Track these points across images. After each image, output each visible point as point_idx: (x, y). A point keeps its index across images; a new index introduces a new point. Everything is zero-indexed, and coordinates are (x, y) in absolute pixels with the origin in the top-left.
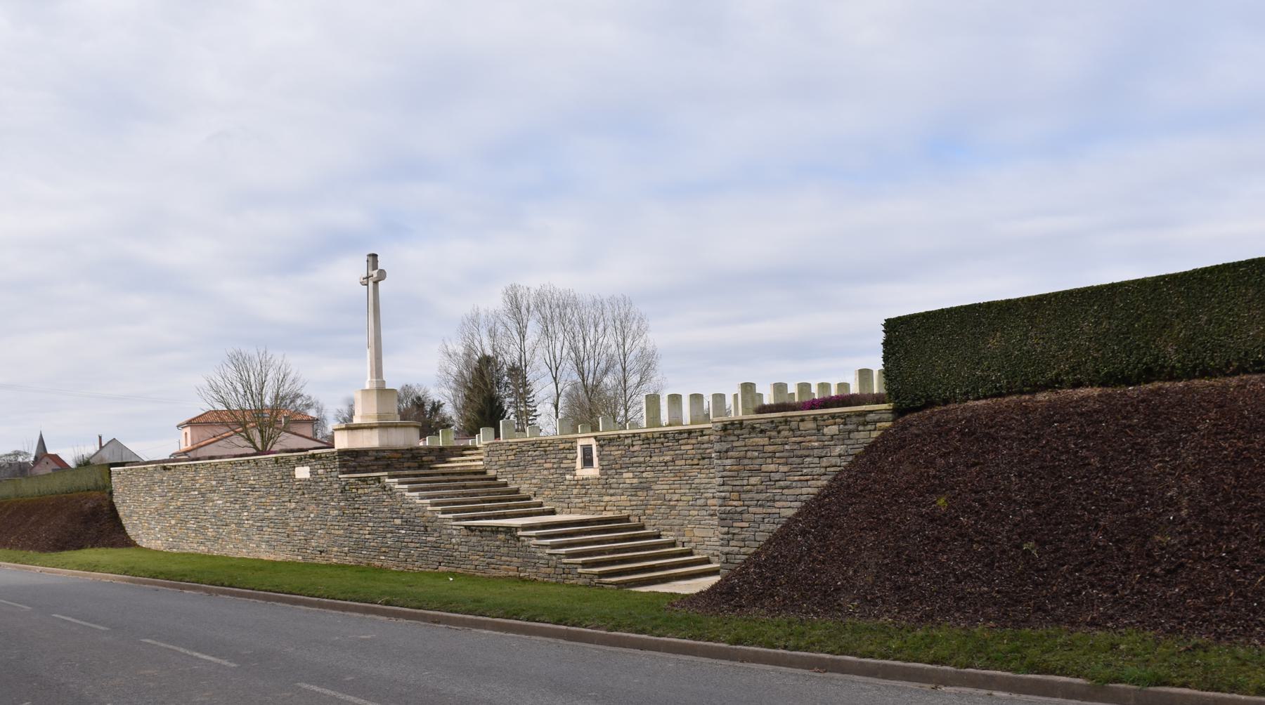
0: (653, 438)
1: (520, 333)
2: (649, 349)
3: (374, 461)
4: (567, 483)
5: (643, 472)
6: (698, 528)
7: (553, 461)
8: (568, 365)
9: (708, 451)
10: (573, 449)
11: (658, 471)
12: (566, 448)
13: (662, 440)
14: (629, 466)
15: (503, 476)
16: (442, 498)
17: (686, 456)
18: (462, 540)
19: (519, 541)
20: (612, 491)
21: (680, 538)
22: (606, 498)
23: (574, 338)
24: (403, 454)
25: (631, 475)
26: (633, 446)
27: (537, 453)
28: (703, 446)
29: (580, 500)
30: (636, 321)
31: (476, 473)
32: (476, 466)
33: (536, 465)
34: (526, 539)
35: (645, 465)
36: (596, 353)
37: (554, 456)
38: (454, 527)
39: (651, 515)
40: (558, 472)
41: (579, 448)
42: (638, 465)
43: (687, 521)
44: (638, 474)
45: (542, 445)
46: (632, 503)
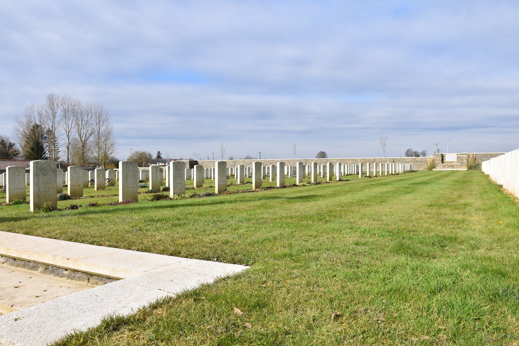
8: (74, 131)
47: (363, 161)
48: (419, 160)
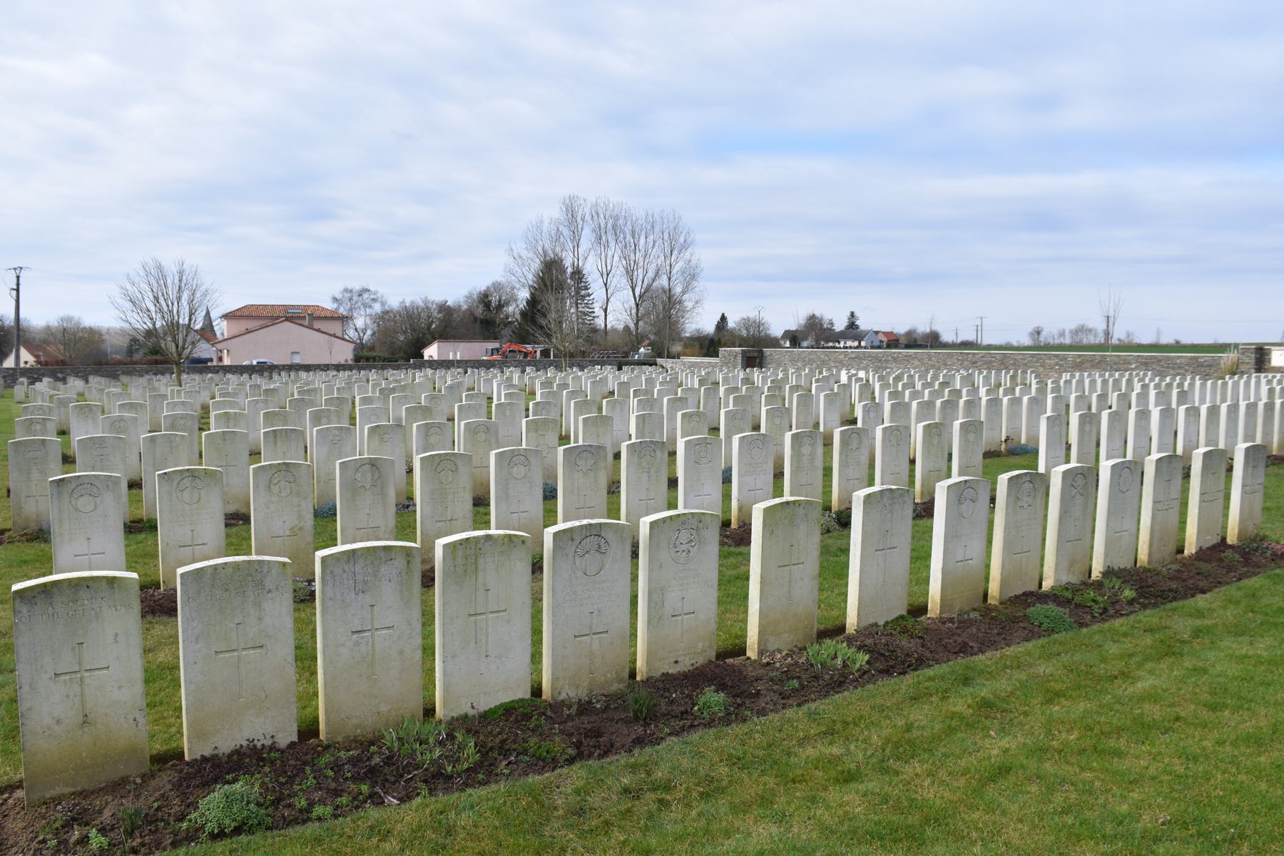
2: (693, 262)
8: (618, 272)
30: (683, 234)
47: (1078, 360)
48: (1206, 361)
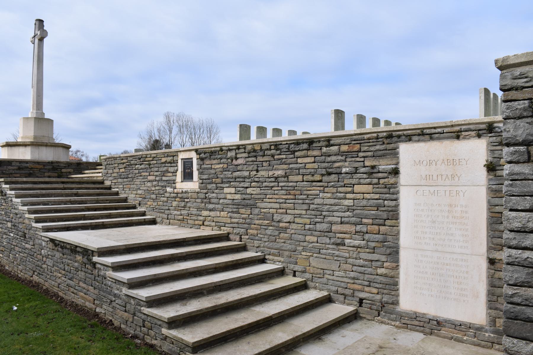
0: (261, 150)
1: (169, 131)
3: (17, 170)
4: (167, 195)
5: (247, 188)
6: (316, 257)
7: (156, 173)
9: (337, 165)
10: (174, 163)
11: (266, 187)
12: (168, 161)
13: (273, 152)
14: (231, 180)
15: (116, 186)
16: (48, 204)
17: (304, 171)
18: (49, 253)
19: (95, 268)
20: (211, 206)
21: (292, 266)
22: (205, 213)
23: (191, 134)
24: (44, 166)
25: (233, 190)
26: (236, 158)
27: (143, 166)
28: (329, 159)
29: (179, 213)
30: (215, 128)
31: (94, 183)
32: (97, 177)
33: (141, 177)
34: (102, 267)
35: (250, 180)
36: (199, 140)
37: (156, 169)
38: (43, 238)
39: (254, 236)
40: (160, 184)
41: (180, 162)
42: (241, 180)
43: (301, 248)
44: (241, 189)
45: (147, 159)
46: (233, 220)
